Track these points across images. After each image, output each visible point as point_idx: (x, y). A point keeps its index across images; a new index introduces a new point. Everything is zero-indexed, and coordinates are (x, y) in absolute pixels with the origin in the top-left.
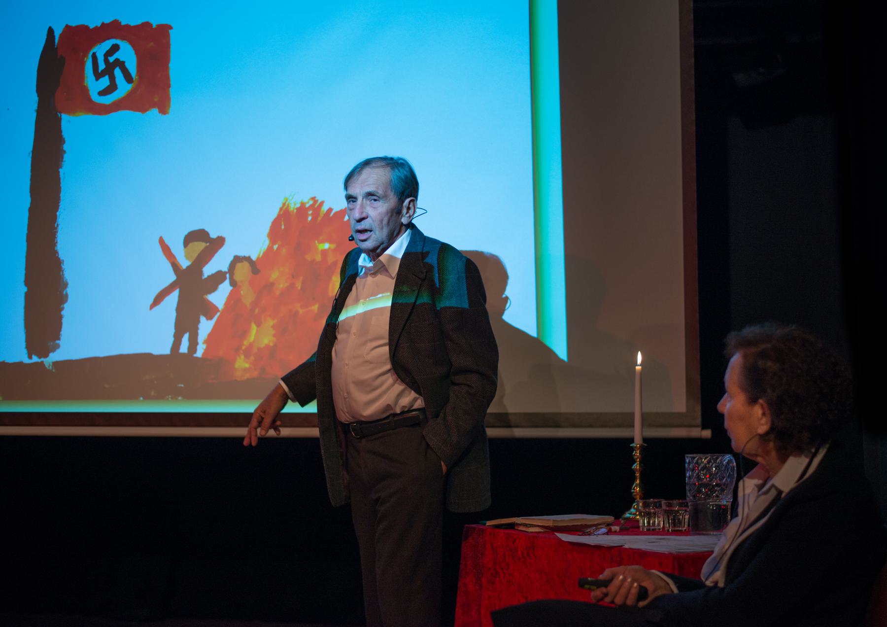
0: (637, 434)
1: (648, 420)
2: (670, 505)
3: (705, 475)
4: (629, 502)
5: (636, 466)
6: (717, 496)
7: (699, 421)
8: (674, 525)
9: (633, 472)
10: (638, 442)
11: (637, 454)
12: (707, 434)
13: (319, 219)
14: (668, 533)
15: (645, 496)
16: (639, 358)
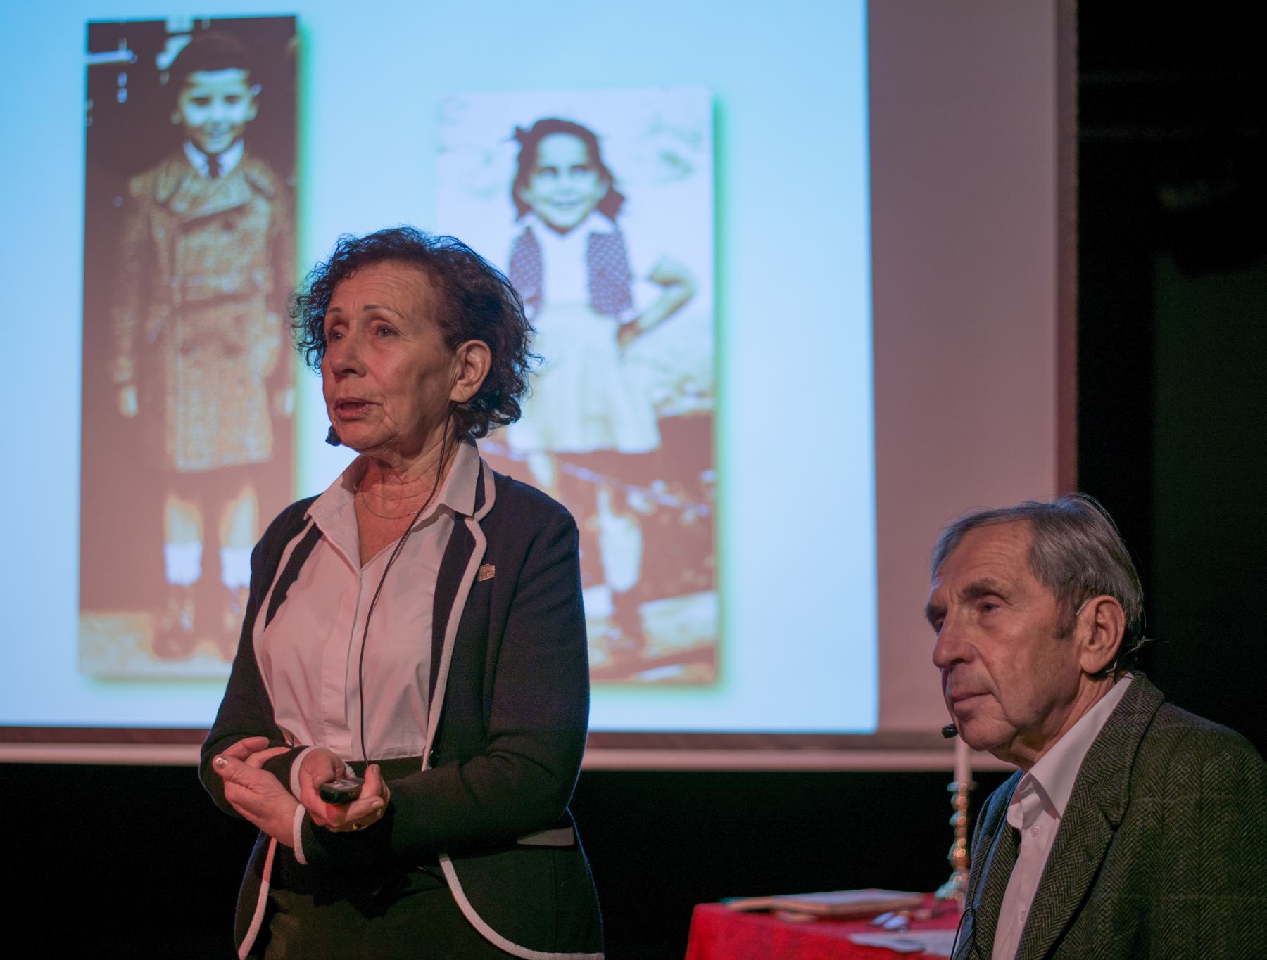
11: (960, 800)
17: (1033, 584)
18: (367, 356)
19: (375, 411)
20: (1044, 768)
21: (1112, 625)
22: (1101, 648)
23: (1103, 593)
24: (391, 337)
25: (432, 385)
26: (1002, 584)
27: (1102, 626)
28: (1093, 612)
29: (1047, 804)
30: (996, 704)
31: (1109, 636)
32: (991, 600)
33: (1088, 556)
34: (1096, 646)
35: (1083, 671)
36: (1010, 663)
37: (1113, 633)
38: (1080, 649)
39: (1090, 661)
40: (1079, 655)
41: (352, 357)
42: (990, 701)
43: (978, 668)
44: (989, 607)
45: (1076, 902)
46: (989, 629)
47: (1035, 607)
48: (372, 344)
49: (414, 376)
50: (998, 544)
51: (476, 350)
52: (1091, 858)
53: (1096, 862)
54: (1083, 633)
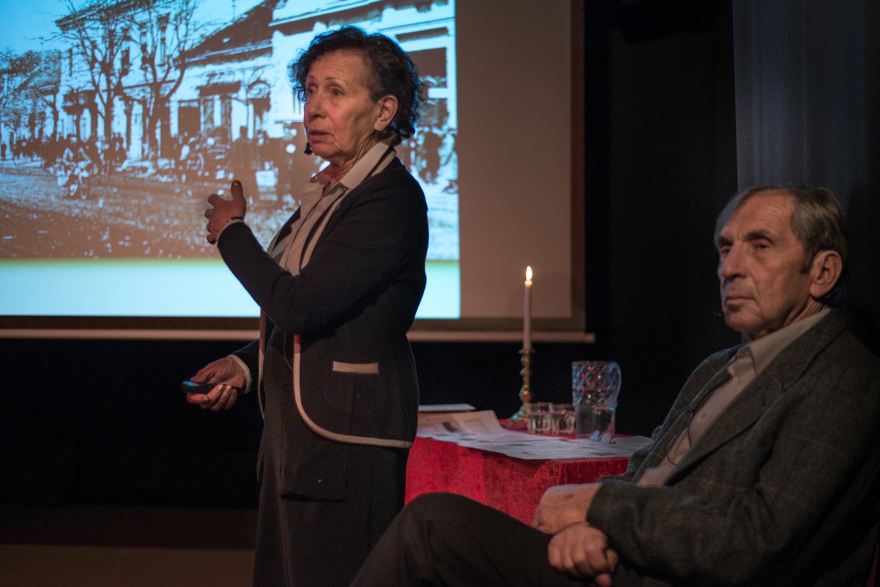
0: (526, 338)
1: (538, 325)
2: (556, 409)
3: (591, 381)
4: (516, 405)
5: (524, 371)
6: (603, 402)
7: (583, 325)
8: (561, 428)
9: (522, 377)
10: (527, 348)
11: (525, 360)
12: (590, 338)
13: (159, 124)
14: (555, 435)
15: (533, 400)
16: (529, 273)
17: (792, 239)
18: (327, 106)
19: (330, 139)
20: (756, 346)
21: (832, 269)
22: (824, 283)
24: (340, 96)
25: (363, 122)
26: (773, 232)
27: (827, 269)
29: (754, 365)
31: (829, 277)
33: (827, 224)
34: (821, 281)
35: (811, 295)
36: (770, 282)
37: (832, 274)
38: (812, 282)
40: (810, 286)
41: (319, 108)
42: (751, 304)
43: (749, 282)
44: (763, 247)
46: (760, 260)
48: (330, 99)
49: (352, 119)
50: (772, 208)
51: (390, 101)
54: (815, 271)
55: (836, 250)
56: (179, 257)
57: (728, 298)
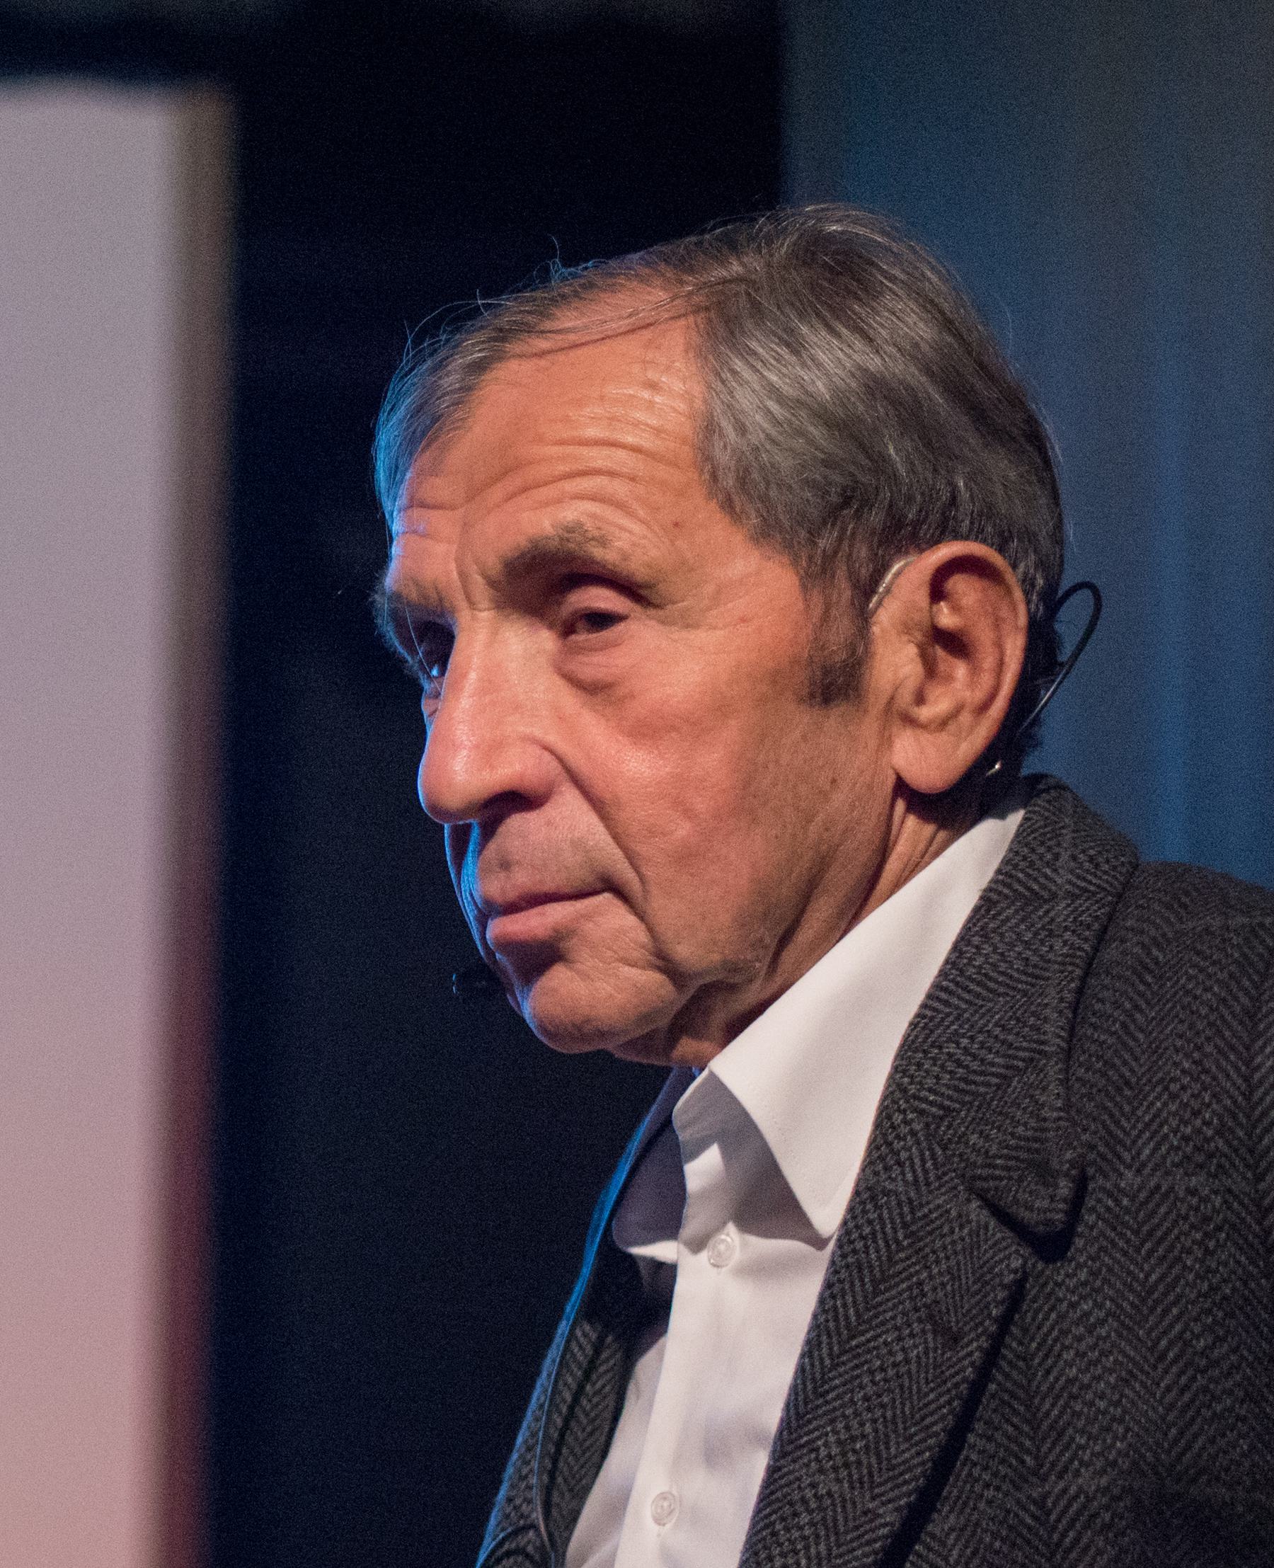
23: (946, 531)
26: (629, 541)
28: (922, 597)
30: (631, 920)
32: (601, 598)
35: (902, 788)
37: (988, 662)
39: (931, 759)
44: (601, 620)
45: (914, 1480)
47: (737, 608)
52: (955, 1339)
53: (974, 1348)
54: (895, 662)
55: (976, 534)
56: (557, 268)
57: (489, 910)
